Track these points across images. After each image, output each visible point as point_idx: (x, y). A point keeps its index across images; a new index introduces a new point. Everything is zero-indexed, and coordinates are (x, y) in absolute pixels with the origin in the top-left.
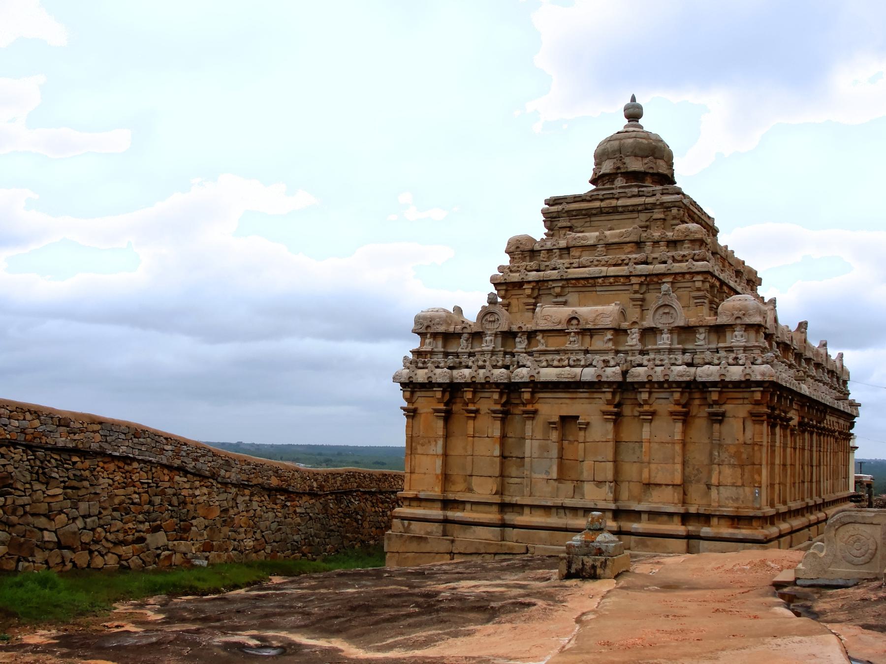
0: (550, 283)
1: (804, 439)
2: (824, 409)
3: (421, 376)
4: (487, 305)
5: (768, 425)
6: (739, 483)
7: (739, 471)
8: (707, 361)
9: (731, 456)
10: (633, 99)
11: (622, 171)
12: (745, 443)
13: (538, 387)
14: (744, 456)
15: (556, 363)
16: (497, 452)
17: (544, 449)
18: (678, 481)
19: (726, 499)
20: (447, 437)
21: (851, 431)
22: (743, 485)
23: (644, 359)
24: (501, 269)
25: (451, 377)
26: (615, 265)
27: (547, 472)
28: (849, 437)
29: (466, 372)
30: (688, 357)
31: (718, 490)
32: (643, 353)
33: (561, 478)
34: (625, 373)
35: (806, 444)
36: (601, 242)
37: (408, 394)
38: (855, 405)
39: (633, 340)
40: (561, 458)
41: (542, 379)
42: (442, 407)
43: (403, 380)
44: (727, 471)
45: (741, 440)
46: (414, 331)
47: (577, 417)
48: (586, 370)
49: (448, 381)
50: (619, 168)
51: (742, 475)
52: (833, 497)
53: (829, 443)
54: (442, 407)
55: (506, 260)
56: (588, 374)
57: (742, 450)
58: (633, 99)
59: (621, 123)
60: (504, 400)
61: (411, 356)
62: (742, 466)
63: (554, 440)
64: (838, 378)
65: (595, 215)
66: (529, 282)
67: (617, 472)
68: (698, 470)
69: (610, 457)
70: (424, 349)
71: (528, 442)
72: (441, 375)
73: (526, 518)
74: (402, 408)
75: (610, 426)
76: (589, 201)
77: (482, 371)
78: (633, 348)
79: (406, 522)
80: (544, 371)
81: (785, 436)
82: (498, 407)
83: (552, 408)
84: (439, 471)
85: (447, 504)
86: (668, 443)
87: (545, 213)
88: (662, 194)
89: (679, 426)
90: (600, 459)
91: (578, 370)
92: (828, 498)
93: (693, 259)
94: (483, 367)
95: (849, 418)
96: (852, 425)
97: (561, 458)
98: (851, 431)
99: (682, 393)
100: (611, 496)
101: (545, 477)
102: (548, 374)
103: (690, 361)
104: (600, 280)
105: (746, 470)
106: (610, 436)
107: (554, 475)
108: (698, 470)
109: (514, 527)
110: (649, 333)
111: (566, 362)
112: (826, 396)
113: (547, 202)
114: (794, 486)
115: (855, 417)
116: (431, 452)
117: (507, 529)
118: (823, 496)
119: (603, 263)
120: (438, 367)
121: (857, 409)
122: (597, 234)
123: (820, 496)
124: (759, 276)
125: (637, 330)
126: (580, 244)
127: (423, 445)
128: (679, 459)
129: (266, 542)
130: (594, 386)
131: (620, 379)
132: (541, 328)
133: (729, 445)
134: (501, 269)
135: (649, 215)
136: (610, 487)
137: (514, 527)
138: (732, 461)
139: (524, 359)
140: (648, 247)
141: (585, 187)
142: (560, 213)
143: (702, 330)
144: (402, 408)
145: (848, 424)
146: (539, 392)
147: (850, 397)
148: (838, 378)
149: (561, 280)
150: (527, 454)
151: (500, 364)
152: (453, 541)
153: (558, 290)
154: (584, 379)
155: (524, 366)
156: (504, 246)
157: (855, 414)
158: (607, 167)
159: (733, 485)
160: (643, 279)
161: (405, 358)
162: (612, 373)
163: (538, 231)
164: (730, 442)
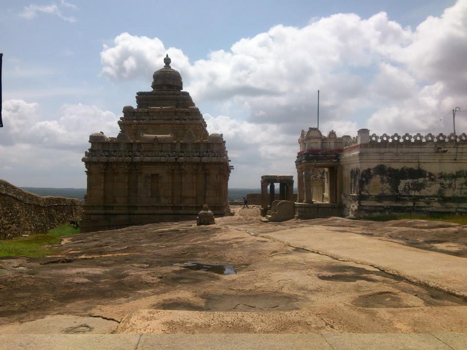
3: (95, 159)
10: (167, 56)
13: (142, 163)
16: (127, 188)
18: (195, 196)
23: (183, 154)
24: (121, 118)
25: (108, 160)
29: (114, 158)
30: (198, 154)
32: (182, 152)
34: (176, 159)
37: (88, 166)
39: (178, 148)
41: (145, 161)
42: (103, 171)
43: (86, 161)
46: (89, 142)
49: (106, 161)
54: (103, 171)
56: (163, 159)
58: (167, 56)
60: (129, 168)
61: (88, 151)
65: (156, 100)
70: (94, 149)
71: (139, 183)
73: (138, 211)
77: (120, 158)
79: (88, 216)
80: (146, 158)
82: (127, 171)
83: (148, 171)
85: (105, 208)
89: (195, 177)
91: (159, 158)
94: (121, 156)
100: (170, 202)
109: (134, 214)
110: (184, 145)
113: (137, 93)
120: (101, 156)
122: (160, 108)
124: (200, 110)
131: (174, 161)
137: (134, 214)
139: (137, 153)
141: (151, 90)
151: (127, 155)
154: (161, 161)
155: (137, 156)
158: (159, 82)
160: (178, 125)
162: (172, 159)
163: (135, 106)
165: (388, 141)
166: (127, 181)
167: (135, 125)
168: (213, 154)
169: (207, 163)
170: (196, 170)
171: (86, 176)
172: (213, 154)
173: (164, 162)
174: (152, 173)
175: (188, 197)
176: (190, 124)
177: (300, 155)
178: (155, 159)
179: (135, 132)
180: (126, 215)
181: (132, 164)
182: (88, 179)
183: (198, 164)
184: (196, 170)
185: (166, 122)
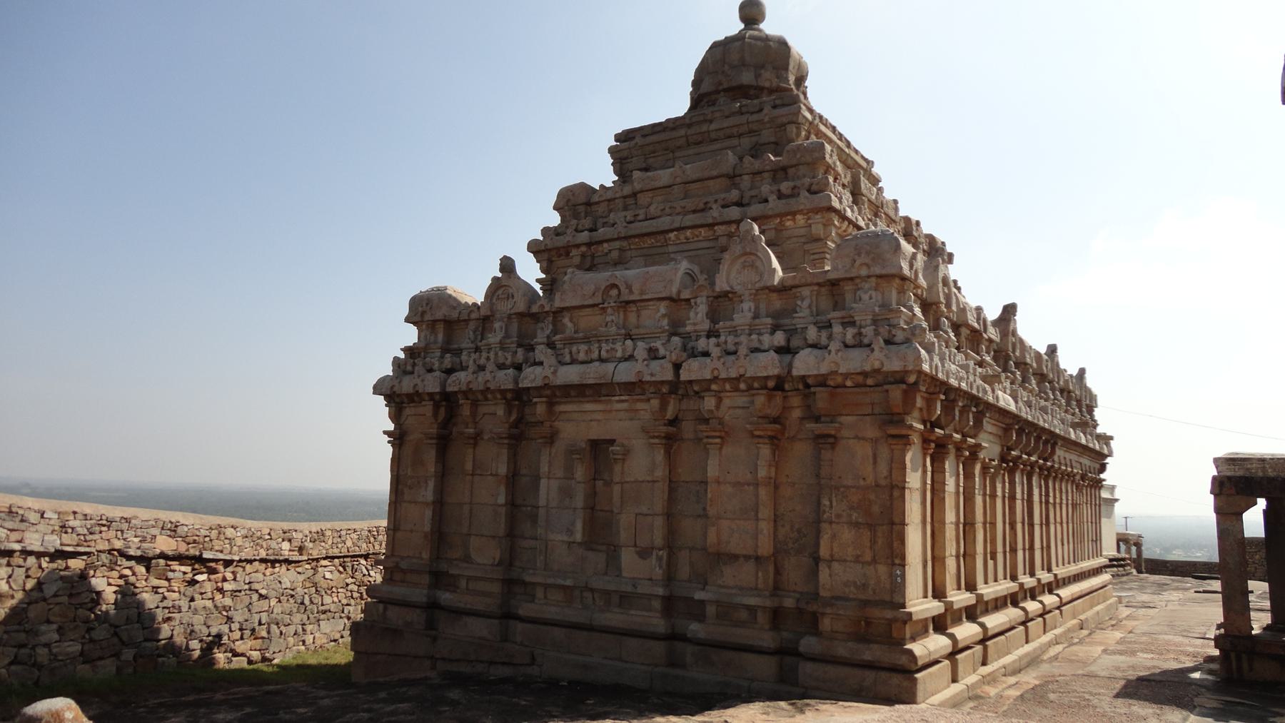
0: (605, 245)
1: (1012, 483)
2: (1051, 440)
3: (407, 386)
4: (500, 275)
5: (925, 450)
6: (868, 557)
7: (867, 534)
8: (810, 342)
9: (852, 508)
11: (725, 86)
12: (877, 486)
13: (558, 394)
14: (876, 509)
15: (582, 356)
17: (566, 493)
19: (846, 584)
20: (443, 476)
21: (1102, 476)
22: (874, 561)
24: (545, 231)
26: (694, 212)
27: (570, 532)
28: (1098, 484)
31: (830, 567)
33: (590, 543)
35: (1018, 490)
36: (678, 180)
38: (1106, 439)
40: (592, 509)
44: (847, 535)
45: (870, 480)
47: (614, 441)
48: (623, 366)
50: (720, 83)
51: (873, 542)
52: (1073, 569)
53: (1063, 494)
55: (554, 220)
56: (625, 373)
57: (872, 497)
59: (734, 26)
61: (402, 355)
62: (871, 527)
63: (579, 479)
64: (1079, 402)
66: (578, 246)
67: (672, 533)
68: (799, 531)
69: (659, 507)
71: (543, 482)
72: (431, 384)
74: (385, 432)
75: (660, 456)
76: (673, 129)
78: (697, 328)
81: (969, 476)
84: (427, 528)
86: (749, 485)
87: (612, 151)
88: (775, 107)
89: (765, 451)
90: (644, 510)
92: (1062, 571)
93: (809, 191)
95: (1100, 460)
96: (1103, 468)
97: (592, 509)
98: (1102, 476)
99: (770, 398)
100: (658, 573)
101: (566, 538)
102: (570, 374)
103: (783, 343)
104: (672, 235)
105: (879, 534)
106: (660, 473)
107: (578, 537)
108: (799, 531)
111: (595, 355)
112: (1054, 422)
114: (994, 557)
115: (1106, 456)
116: (421, 499)
117: (512, 622)
118: (1056, 570)
119: (679, 210)
121: (1108, 445)
123: (1049, 570)
125: (704, 299)
126: (649, 187)
127: (410, 488)
128: (765, 512)
129: (123, 643)
130: (633, 388)
132: (567, 305)
133: (847, 487)
134: (545, 231)
135: (754, 139)
136: (659, 559)
138: (855, 515)
140: (746, 181)
142: (634, 149)
143: (806, 292)
144: (385, 432)
145: (1097, 466)
146: (559, 403)
147: (1099, 430)
148: (1077, 398)
149: (618, 239)
150: (542, 502)
151: (508, 362)
152: (435, 639)
153: (615, 254)
154: (617, 379)
156: (553, 199)
157: (1106, 451)
159: (857, 559)
161: (396, 360)
162: (662, 371)
164: (850, 483)
165: (212, 662)
166: (503, 470)
167: (584, 249)
168: (850, 332)
169: (822, 381)
170: (775, 420)
171: (386, 451)
172: (850, 332)
173: (633, 384)
174: (594, 436)
175: (735, 557)
176: (782, 215)
177: (1214, 478)
178: (592, 373)
179: (777, 303)
180: (489, 617)
181: (519, 398)
182: (397, 463)
183: (780, 384)
184: (775, 420)
185: (690, 220)
